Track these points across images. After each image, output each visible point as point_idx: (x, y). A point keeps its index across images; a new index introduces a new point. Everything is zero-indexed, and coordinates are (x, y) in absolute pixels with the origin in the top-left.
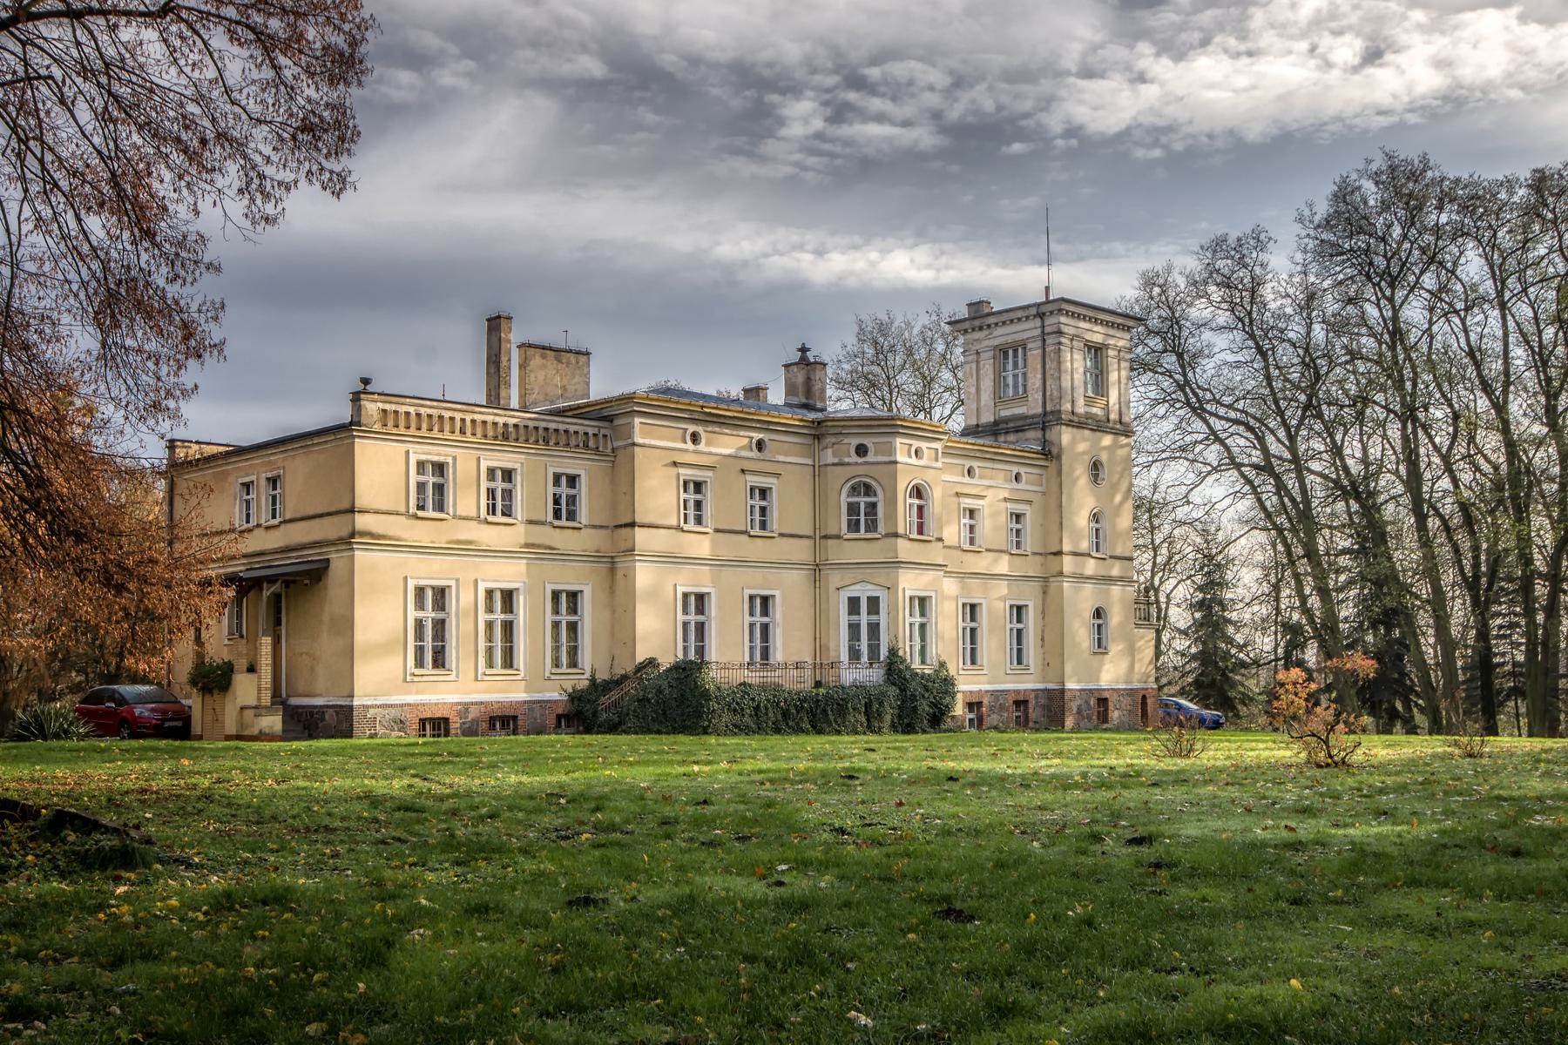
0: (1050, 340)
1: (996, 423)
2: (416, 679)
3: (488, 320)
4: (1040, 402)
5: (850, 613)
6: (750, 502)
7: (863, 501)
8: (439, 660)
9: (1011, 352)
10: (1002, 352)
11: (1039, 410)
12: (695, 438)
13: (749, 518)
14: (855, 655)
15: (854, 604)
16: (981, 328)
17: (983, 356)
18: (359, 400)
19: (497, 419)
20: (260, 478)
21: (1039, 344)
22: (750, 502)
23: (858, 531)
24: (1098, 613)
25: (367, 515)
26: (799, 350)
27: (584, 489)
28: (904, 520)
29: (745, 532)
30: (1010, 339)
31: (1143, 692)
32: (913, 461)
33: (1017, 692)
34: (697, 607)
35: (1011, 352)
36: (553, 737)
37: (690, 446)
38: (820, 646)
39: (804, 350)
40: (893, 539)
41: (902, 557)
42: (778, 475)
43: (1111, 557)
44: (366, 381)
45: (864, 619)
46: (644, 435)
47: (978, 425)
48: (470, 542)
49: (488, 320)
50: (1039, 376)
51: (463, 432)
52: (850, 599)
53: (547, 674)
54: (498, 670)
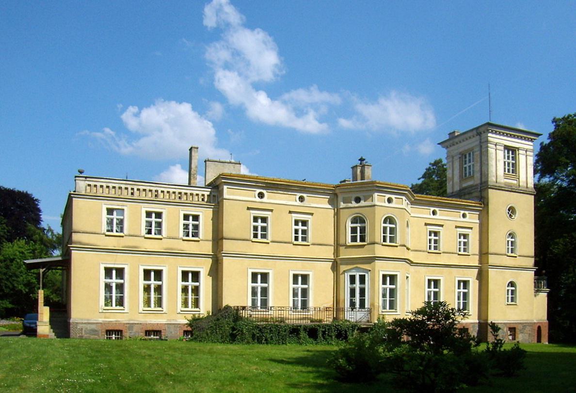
1: (460, 190)
2: (104, 311)
4: (479, 177)
6: (459, 240)
7: (358, 225)
8: (120, 302)
11: (479, 182)
12: (261, 195)
14: (353, 305)
15: (352, 279)
17: (455, 158)
19: (158, 189)
22: (459, 240)
23: (356, 241)
26: (359, 160)
27: (201, 222)
29: (505, 255)
30: (466, 148)
31: (538, 325)
38: (337, 300)
40: (372, 246)
41: (378, 254)
42: (271, 211)
43: (443, 253)
45: (357, 285)
47: (453, 193)
48: (136, 247)
50: (479, 164)
52: (351, 276)
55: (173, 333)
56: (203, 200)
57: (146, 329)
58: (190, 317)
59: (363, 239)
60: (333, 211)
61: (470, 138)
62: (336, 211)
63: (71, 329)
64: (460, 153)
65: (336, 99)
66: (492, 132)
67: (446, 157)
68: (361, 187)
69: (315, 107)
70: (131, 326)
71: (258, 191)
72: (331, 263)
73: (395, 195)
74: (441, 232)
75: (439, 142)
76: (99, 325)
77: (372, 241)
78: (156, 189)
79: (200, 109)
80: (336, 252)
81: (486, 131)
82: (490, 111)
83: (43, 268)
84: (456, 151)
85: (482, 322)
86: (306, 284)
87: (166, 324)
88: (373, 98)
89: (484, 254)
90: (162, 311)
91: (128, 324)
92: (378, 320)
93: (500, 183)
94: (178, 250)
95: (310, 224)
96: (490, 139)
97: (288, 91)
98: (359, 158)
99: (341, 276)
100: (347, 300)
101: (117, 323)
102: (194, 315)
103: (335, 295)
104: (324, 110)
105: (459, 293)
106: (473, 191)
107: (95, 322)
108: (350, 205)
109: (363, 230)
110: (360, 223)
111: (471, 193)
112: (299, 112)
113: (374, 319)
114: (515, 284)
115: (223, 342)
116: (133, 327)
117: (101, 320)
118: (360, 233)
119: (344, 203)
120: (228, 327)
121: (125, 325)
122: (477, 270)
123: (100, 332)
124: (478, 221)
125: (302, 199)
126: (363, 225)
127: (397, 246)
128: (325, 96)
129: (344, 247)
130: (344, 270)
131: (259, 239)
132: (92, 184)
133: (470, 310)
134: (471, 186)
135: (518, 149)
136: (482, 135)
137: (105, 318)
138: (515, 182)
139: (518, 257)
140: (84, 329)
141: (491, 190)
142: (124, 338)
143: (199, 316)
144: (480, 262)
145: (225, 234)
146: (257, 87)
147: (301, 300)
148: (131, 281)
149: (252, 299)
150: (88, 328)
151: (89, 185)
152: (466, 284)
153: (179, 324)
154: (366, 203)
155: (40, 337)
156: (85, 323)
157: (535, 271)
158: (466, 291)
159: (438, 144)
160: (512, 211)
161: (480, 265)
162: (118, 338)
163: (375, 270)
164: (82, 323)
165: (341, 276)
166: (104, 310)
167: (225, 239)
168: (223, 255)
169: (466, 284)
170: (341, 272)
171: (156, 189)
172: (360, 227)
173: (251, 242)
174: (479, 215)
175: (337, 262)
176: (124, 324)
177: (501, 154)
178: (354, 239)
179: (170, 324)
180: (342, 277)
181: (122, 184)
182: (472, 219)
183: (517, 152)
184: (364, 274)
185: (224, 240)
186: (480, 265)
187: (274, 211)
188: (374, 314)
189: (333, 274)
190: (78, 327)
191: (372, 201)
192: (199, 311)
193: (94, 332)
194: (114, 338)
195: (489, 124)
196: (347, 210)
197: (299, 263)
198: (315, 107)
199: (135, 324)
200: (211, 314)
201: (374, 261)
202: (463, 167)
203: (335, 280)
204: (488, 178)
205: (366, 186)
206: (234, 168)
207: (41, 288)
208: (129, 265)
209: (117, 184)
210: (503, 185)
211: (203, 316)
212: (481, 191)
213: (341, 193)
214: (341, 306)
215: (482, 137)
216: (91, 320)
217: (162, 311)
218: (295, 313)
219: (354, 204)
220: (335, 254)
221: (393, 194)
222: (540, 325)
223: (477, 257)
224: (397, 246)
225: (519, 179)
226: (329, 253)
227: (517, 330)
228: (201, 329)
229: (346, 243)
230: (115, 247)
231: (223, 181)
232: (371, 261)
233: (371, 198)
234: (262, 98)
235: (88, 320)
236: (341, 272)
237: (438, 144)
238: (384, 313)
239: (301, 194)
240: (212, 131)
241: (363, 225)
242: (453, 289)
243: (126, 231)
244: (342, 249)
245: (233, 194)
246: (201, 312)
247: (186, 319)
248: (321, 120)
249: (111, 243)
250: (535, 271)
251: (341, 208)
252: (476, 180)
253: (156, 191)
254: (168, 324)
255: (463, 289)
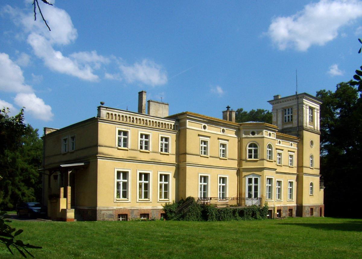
0: (300, 105)
2: (117, 201)
3: (139, 93)
4: (297, 123)
5: (249, 183)
6: (220, 148)
7: (253, 148)
8: (125, 195)
9: (287, 110)
10: (284, 110)
11: (296, 126)
12: (205, 127)
13: (220, 153)
14: (250, 196)
15: (250, 181)
16: (278, 103)
18: (100, 109)
19: (144, 118)
20: (69, 137)
21: (296, 106)
24: (312, 184)
25: (102, 147)
26: (227, 107)
28: (266, 155)
30: (287, 105)
32: (268, 137)
33: (290, 206)
34: (123, 195)
35: (287, 110)
36: (176, 223)
37: (203, 130)
38: (240, 193)
39: (228, 107)
42: (228, 140)
43: (229, 159)
44: (102, 104)
46: (189, 125)
49: (139, 93)
51: (133, 121)
53: (158, 201)
54: (121, 198)
55: (155, 215)
56: (171, 128)
57: (141, 213)
58: (164, 204)
59: (256, 157)
60: (237, 139)
61: (290, 100)
62: (239, 139)
63: (98, 214)
64: (283, 108)
65: (105, 60)
66: (305, 99)
67: (272, 109)
68: (257, 126)
69: (92, 65)
70: (132, 211)
71: (204, 124)
72: (236, 171)
73: (272, 131)
74: (294, 156)
75: (270, 100)
76: (114, 211)
77: (262, 158)
78: (130, 116)
79: (13, 57)
80: (240, 164)
81: (302, 97)
82: (297, 85)
83: (70, 171)
84: (281, 107)
85: (298, 205)
86: (126, 179)
87: (151, 209)
88: (130, 62)
89: (300, 167)
90: (149, 201)
91: (131, 210)
92: (265, 205)
93: (308, 127)
94: (158, 161)
95: (129, 134)
96: (304, 102)
97: (77, 52)
98: (227, 106)
99: (243, 178)
100: (247, 193)
101: (125, 209)
102: (166, 203)
103: (239, 190)
104: (98, 66)
105: (201, 185)
106: (292, 131)
107: (112, 209)
108: (248, 136)
109: (256, 151)
110: (254, 147)
111: (291, 132)
112: (82, 66)
113: (263, 205)
114: (313, 184)
115: (198, 220)
116: (133, 211)
117: (115, 208)
118: (254, 153)
119: (245, 135)
120: (199, 211)
121: (129, 211)
122: (296, 176)
123: (115, 216)
124: (297, 148)
125: (223, 131)
126: (256, 148)
127: (272, 162)
128: (101, 59)
129: (245, 161)
130: (245, 175)
131: (203, 155)
132: (110, 112)
133: (293, 198)
134: (291, 128)
135: (314, 108)
136: (299, 99)
137: (117, 206)
138: (312, 127)
139: (314, 169)
140: (105, 214)
141: (305, 131)
142: (128, 220)
143: (169, 204)
144: (298, 171)
145: (188, 151)
146: (56, 47)
147: (123, 191)
148: (132, 181)
149: (160, 192)
150: (108, 213)
151: (108, 113)
152: (166, 177)
153: (158, 209)
154: (258, 135)
155: (68, 220)
156: (106, 210)
157: (320, 177)
158: (206, 184)
159: (268, 102)
160: (312, 143)
161: (298, 173)
162: (124, 220)
163: (264, 176)
164: (104, 210)
165: (243, 178)
166: (117, 200)
167: (188, 154)
168: (187, 164)
169: (166, 177)
170: (243, 177)
171: (130, 116)
172: (254, 150)
173: (200, 156)
174: (297, 144)
175: (239, 170)
176: (129, 210)
177: (308, 110)
178: (250, 157)
179: (154, 209)
180: (244, 179)
181: (163, 120)
182: (294, 147)
183: (314, 110)
184: (257, 177)
185: (187, 155)
186: (298, 173)
187: (211, 137)
188: (263, 202)
189: (237, 177)
190: (102, 213)
191: (262, 135)
192: (169, 201)
193: (111, 216)
194: (121, 220)
195: (305, 94)
196: (247, 139)
197: (222, 171)
198: (92, 65)
199: (135, 210)
200: (175, 202)
201: (263, 170)
202: (284, 116)
203: (239, 181)
204: (303, 124)
205: (260, 125)
206: (165, 107)
207: (69, 185)
208: (131, 170)
209: (148, 119)
210: (309, 129)
211: (171, 204)
212: (298, 131)
213: (243, 128)
214: (243, 196)
215: (299, 101)
216: (109, 208)
217: (149, 201)
218: (220, 201)
219: (251, 136)
220: (239, 165)
221: (271, 131)
222: (321, 206)
223: (296, 169)
224: (272, 162)
225: (314, 125)
226: (235, 164)
227: (313, 210)
228: (171, 212)
229: (246, 159)
230: (123, 157)
231: (187, 117)
232: (262, 170)
233: (261, 133)
234: (59, 55)
235: (107, 208)
236: (243, 177)
237: (268, 102)
238: (267, 201)
239: (223, 128)
240: (20, 73)
241: (256, 148)
242: (287, 186)
243: (151, 149)
244: (244, 162)
245: (192, 126)
246: (170, 201)
247: (162, 206)
248: (95, 72)
249: (222, 163)
250: (320, 177)
251: (243, 138)
252: (295, 124)
253: (146, 120)
254: (153, 209)
255: (204, 182)
